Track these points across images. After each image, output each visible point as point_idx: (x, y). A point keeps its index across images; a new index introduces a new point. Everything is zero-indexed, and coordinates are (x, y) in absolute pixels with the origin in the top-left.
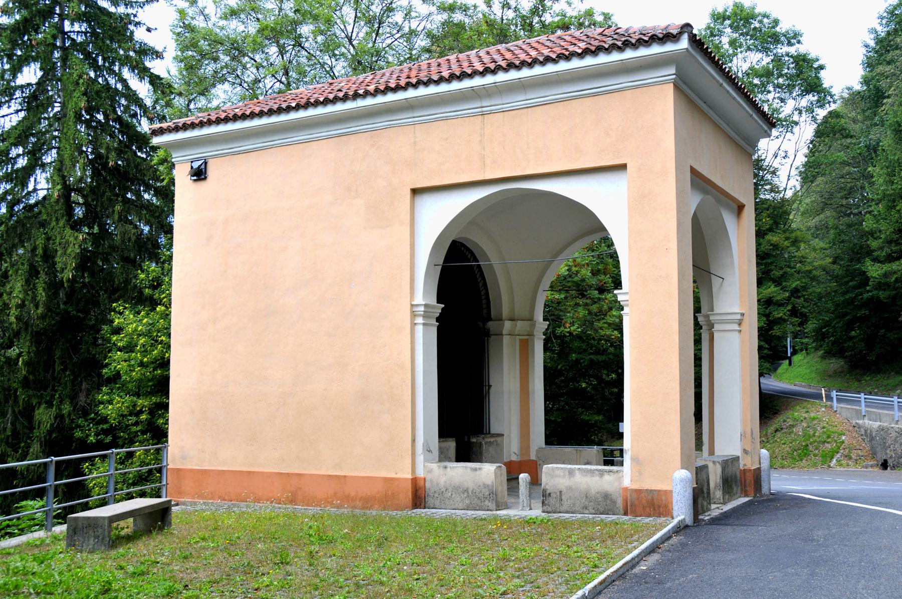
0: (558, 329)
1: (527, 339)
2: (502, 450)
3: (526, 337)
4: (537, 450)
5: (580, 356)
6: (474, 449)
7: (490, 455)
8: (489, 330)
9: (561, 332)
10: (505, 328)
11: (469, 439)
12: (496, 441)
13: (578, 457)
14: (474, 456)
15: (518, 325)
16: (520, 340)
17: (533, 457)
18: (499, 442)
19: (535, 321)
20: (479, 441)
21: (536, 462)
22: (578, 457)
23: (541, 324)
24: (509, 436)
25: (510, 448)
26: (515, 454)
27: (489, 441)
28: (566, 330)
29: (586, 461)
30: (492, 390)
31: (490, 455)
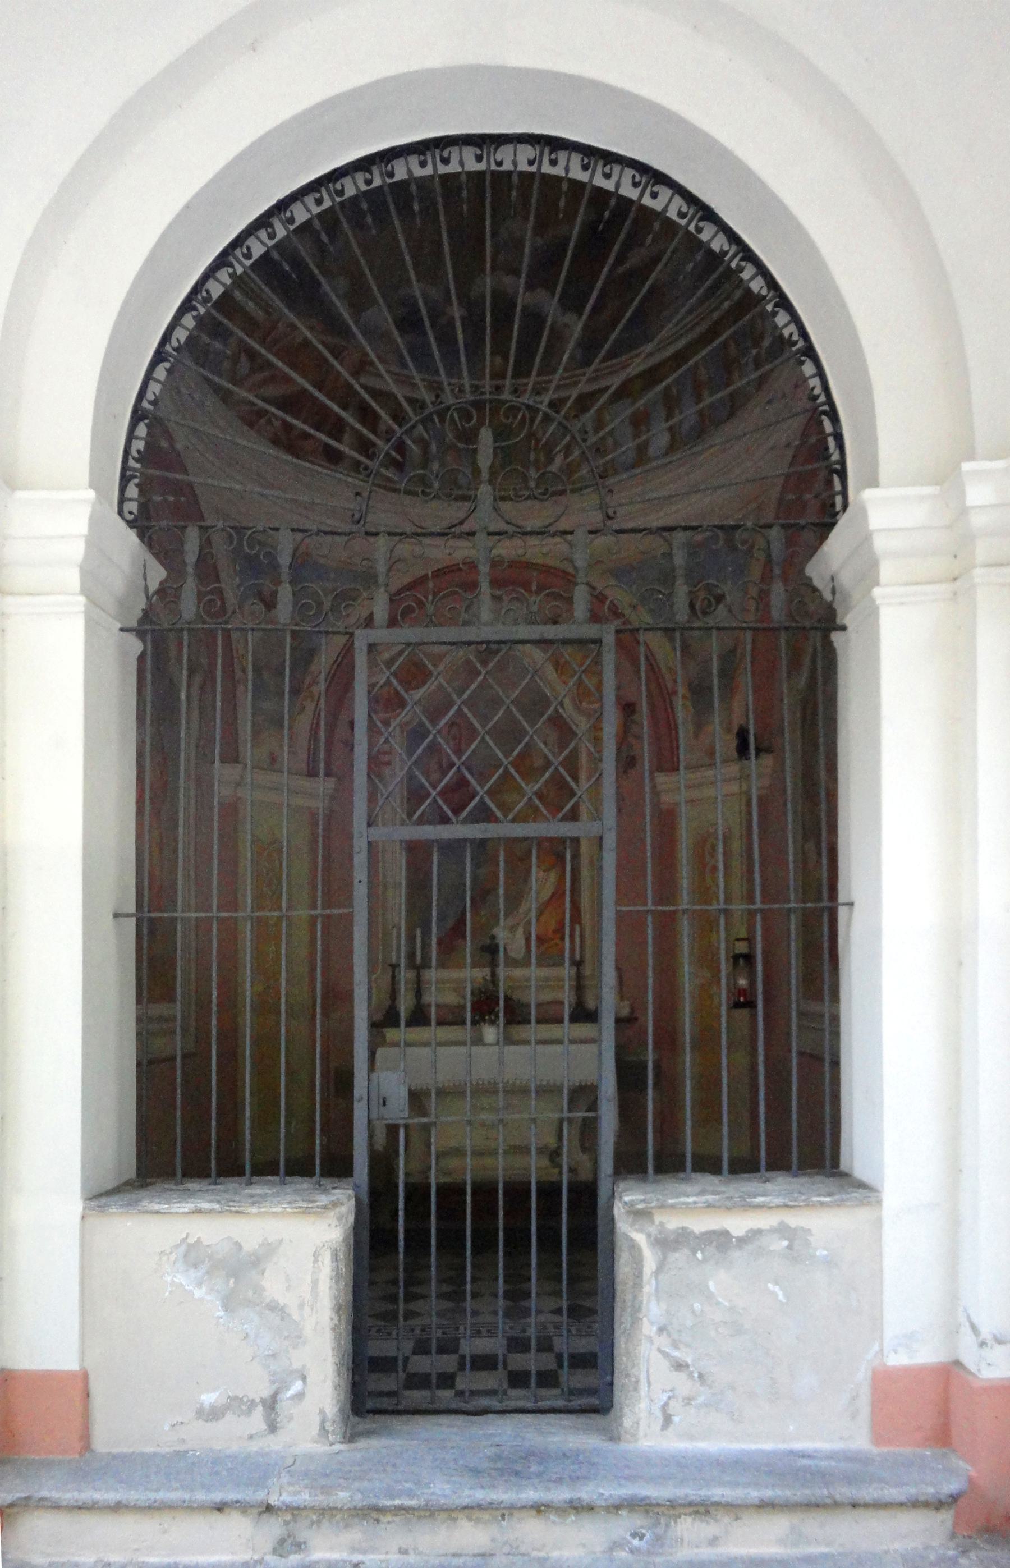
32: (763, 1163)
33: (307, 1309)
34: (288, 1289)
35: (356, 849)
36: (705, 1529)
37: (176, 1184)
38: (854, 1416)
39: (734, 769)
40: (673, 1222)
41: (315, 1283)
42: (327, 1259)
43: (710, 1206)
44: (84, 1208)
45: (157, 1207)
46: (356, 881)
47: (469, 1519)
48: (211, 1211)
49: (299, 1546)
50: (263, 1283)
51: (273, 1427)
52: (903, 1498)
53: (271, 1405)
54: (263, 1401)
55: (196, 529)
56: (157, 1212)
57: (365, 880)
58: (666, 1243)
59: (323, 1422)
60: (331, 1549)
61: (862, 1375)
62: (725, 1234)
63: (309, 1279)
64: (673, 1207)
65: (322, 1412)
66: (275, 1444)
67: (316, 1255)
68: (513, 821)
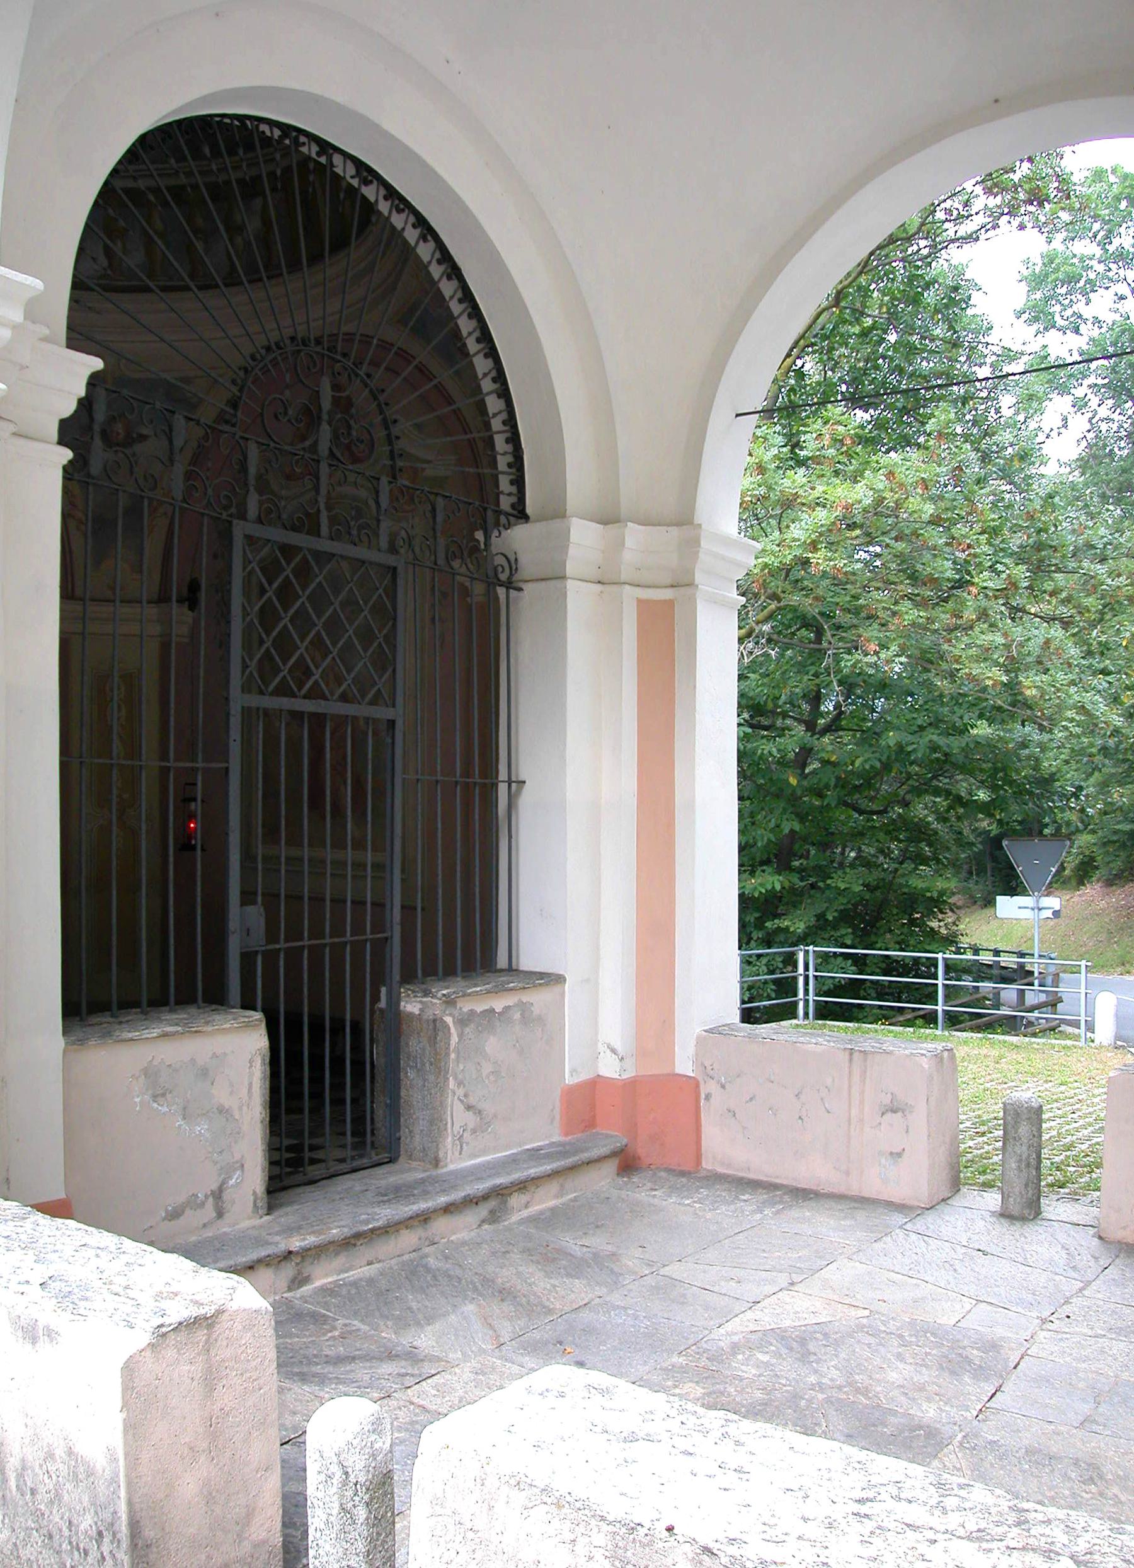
0: (846, 657)
1: (670, 603)
2: (554, 1040)
3: (667, 594)
4: (700, 1041)
5: (910, 738)
6: (413, 1043)
7: (487, 1068)
8: (513, 565)
9: (854, 666)
10: (572, 551)
11: (393, 1001)
12: (524, 1007)
13: (856, 1078)
14: (411, 1074)
15: (629, 543)
16: (643, 606)
17: (684, 1065)
18: (536, 1010)
19: (700, 525)
20: (429, 1014)
21: (693, 1085)
22: (856, 1078)
23: (726, 541)
24: (592, 982)
25: (596, 1034)
26: (614, 1051)
27: (479, 1008)
28: (866, 659)
29: (887, 1100)
30: (527, 800)
31: (487, 1068)
32: (172, 998)
33: (245, 1108)
34: (232, 1093)
35: (232, 712)
36: (523, 1198)
37: (171, 1011)
38: (552, 1122)
39: (152, 611)
40: (466, 1006)
41: (250, 1085)
42: (258, 1062)
43: (488, 992)
44: (66, 1044)
45: (130, 1035)
46: (231, 741)
47: (407, 1228)
48: (174, 1034)
49: (306, 1280)
50: (213, 1091)
51: (220, 1214)
52: (608, 1152)
53: (218, 1195)
54: (213, 1193)
55: (104, 392)
56: (132, 1040)
57: (239, 740)
58: (463, 1022)
59: (255, 1202)
60: (327, 1275)
61: (557, 1094)
62: (492, 1011)
63: (246, 1083)
64: (469, 995)
65: (254, 1193)
66: (224, 1227)
67: (251, 1062)
68: (305, 697)
